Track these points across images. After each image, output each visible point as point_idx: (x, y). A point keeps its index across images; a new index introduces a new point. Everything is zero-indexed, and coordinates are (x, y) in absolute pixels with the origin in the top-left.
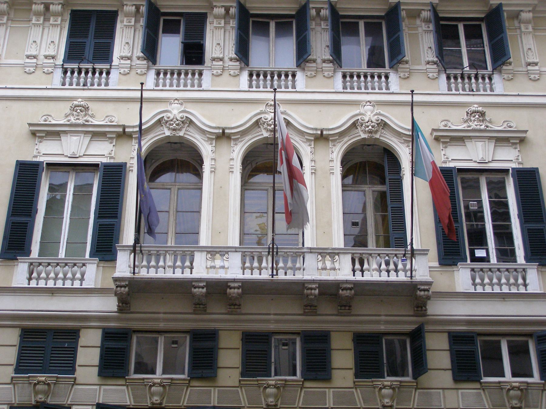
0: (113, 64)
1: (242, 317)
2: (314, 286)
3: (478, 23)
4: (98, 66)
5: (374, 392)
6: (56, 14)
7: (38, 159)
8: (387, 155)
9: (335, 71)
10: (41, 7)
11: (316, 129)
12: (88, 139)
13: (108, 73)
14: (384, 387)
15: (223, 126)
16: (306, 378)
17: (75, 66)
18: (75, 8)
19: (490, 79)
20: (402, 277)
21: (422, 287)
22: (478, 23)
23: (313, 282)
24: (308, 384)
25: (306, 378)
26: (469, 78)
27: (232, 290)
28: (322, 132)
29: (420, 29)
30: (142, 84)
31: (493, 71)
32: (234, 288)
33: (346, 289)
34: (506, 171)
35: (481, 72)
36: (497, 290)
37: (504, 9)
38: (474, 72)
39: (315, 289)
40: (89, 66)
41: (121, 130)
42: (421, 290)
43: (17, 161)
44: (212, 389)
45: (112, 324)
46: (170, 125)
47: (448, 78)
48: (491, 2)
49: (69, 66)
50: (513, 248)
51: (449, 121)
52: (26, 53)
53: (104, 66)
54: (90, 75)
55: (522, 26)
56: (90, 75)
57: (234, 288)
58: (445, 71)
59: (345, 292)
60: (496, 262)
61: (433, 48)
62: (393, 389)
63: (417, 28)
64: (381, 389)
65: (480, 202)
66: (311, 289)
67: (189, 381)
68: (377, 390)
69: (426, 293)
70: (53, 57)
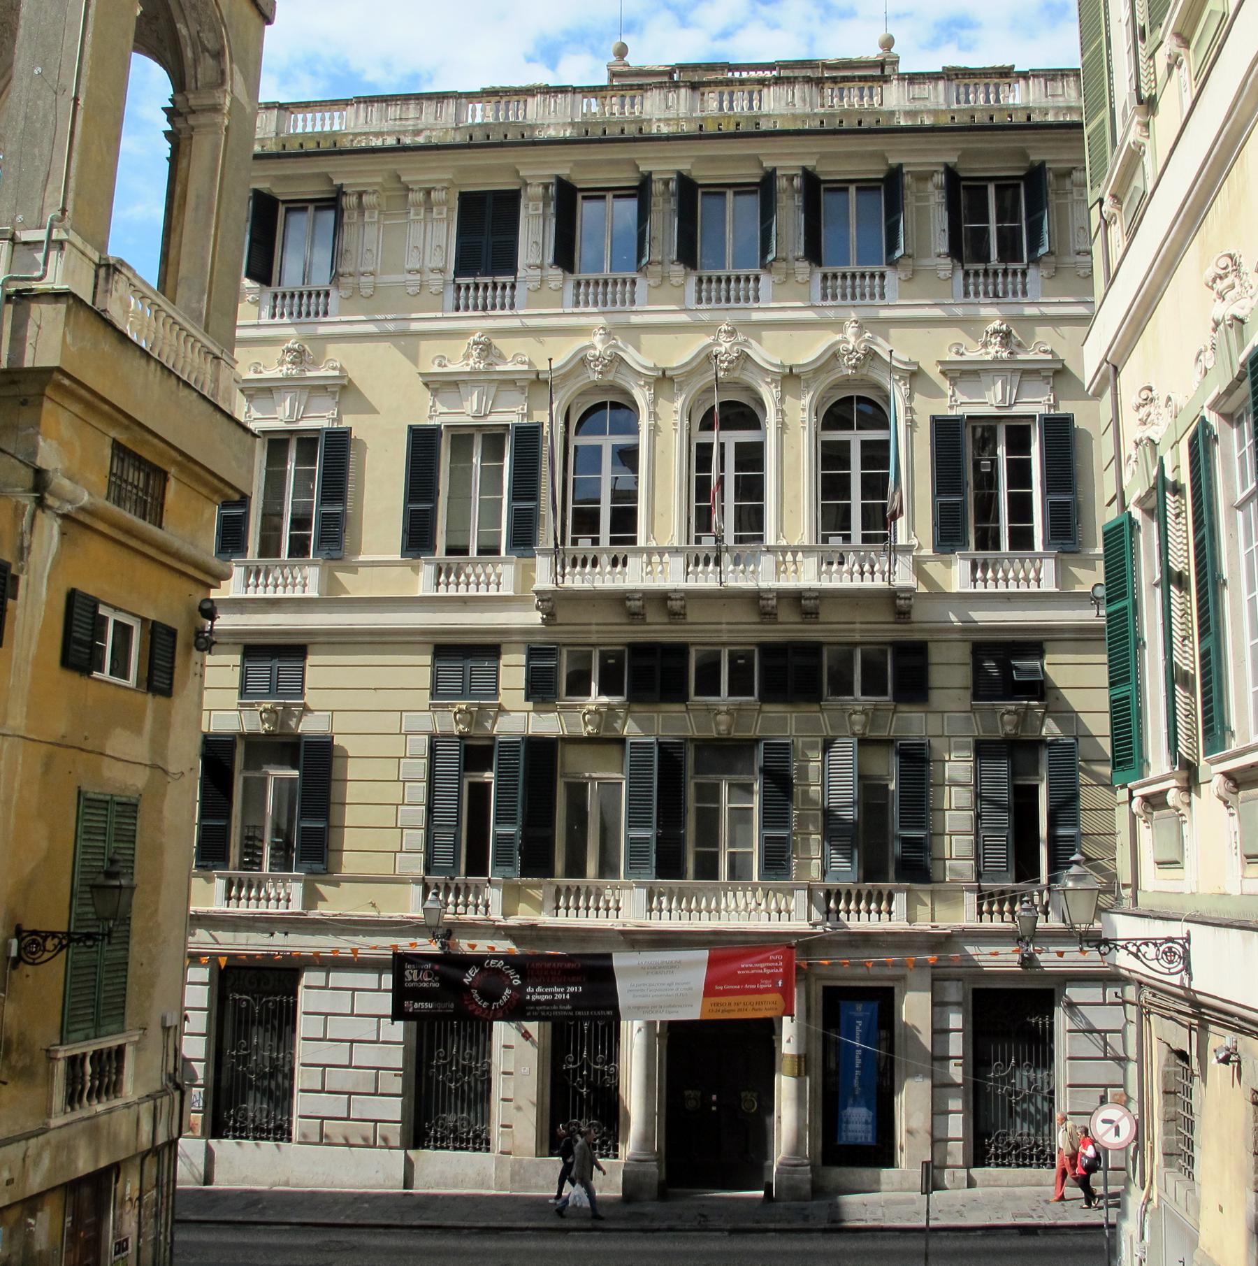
0: (519, 275)
1: (687, 627)
2: (771, 596)
3: (1015, 182)
4: (500, 279)
5: (844, 717)
6: (441, 203)
7: (436, 421)
8: (443, 1112)
9: (811, 273)
10: (420, 196)
11: (783, 366)
12: (493, 391)
13: (513, 287)
14: (855, 713)
15: (663, 366)
16: (764, 699)
17: (470, 280)
18: (464, 190)
19: (1024, 274)
20: (879, 583)
21: (903, 595)
22: (1015, 182)
23: (770, 590)
24: (767, 707)
25: (764, 699)
26: (996, 273)
27: (674, 602)
28: (791, 370)
29: (932, 198)
30: (550, 360)
31: (1028, 265)
32: (676, 600)
33: (810, 598)
34: (1033, 417)
35: (1012, 266)
36: (1002, 589)
37: (1047, 166)
38: (1002, 266)
39: (772, 599)
40: (488, 280)
41: (534, 377)
42: (901, 599)
43: (410, 427)
44: (655, 715)
45: (538, 638)
46: (595, 366)
47: (967, 274)
48: (1032, 158)
49: (463, 281)
50: (713, 849)
51: (961, 345)
52: (407, 267)
53: (508, 279)
54: (490, 292)
55: (1075, 189)
56: (490, 292)
57: (676, 600)
58: (963, 266)
59: (808, 602)
60: (1007, 551)
61: (947, 230)
62: (867, 714)
63: (928, 196)
64: (851, 714)
65: (994, 463)
66: (768, 599)
67: (629, 706)
68: (847, 715)
69: (907, 601)
70: (442, 271)
